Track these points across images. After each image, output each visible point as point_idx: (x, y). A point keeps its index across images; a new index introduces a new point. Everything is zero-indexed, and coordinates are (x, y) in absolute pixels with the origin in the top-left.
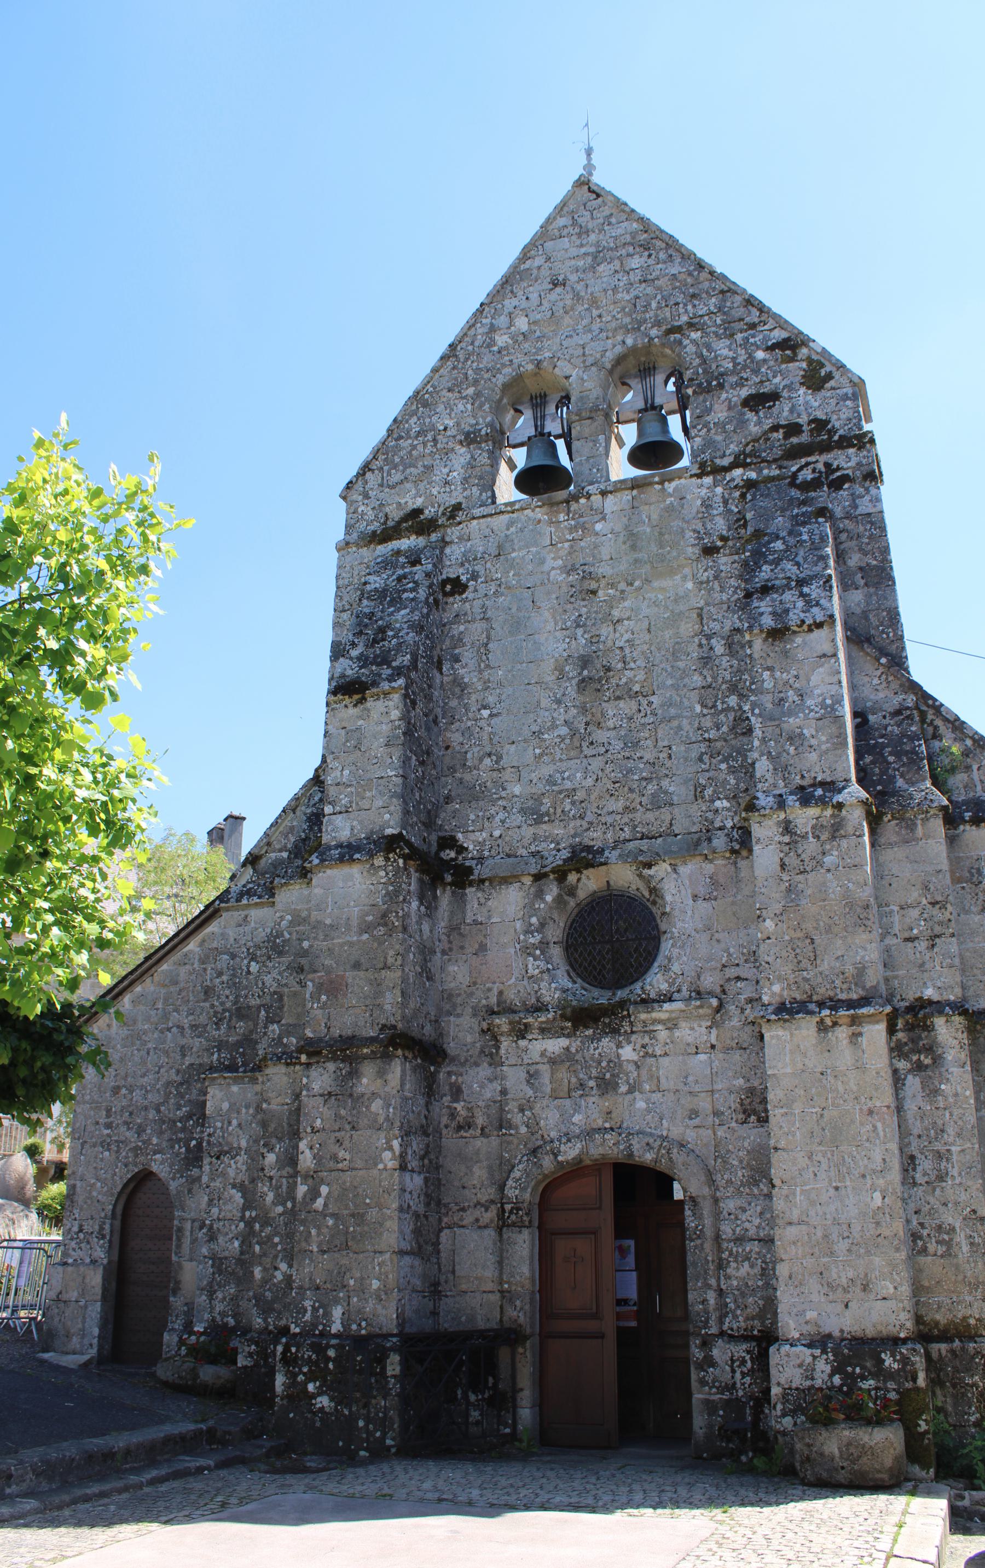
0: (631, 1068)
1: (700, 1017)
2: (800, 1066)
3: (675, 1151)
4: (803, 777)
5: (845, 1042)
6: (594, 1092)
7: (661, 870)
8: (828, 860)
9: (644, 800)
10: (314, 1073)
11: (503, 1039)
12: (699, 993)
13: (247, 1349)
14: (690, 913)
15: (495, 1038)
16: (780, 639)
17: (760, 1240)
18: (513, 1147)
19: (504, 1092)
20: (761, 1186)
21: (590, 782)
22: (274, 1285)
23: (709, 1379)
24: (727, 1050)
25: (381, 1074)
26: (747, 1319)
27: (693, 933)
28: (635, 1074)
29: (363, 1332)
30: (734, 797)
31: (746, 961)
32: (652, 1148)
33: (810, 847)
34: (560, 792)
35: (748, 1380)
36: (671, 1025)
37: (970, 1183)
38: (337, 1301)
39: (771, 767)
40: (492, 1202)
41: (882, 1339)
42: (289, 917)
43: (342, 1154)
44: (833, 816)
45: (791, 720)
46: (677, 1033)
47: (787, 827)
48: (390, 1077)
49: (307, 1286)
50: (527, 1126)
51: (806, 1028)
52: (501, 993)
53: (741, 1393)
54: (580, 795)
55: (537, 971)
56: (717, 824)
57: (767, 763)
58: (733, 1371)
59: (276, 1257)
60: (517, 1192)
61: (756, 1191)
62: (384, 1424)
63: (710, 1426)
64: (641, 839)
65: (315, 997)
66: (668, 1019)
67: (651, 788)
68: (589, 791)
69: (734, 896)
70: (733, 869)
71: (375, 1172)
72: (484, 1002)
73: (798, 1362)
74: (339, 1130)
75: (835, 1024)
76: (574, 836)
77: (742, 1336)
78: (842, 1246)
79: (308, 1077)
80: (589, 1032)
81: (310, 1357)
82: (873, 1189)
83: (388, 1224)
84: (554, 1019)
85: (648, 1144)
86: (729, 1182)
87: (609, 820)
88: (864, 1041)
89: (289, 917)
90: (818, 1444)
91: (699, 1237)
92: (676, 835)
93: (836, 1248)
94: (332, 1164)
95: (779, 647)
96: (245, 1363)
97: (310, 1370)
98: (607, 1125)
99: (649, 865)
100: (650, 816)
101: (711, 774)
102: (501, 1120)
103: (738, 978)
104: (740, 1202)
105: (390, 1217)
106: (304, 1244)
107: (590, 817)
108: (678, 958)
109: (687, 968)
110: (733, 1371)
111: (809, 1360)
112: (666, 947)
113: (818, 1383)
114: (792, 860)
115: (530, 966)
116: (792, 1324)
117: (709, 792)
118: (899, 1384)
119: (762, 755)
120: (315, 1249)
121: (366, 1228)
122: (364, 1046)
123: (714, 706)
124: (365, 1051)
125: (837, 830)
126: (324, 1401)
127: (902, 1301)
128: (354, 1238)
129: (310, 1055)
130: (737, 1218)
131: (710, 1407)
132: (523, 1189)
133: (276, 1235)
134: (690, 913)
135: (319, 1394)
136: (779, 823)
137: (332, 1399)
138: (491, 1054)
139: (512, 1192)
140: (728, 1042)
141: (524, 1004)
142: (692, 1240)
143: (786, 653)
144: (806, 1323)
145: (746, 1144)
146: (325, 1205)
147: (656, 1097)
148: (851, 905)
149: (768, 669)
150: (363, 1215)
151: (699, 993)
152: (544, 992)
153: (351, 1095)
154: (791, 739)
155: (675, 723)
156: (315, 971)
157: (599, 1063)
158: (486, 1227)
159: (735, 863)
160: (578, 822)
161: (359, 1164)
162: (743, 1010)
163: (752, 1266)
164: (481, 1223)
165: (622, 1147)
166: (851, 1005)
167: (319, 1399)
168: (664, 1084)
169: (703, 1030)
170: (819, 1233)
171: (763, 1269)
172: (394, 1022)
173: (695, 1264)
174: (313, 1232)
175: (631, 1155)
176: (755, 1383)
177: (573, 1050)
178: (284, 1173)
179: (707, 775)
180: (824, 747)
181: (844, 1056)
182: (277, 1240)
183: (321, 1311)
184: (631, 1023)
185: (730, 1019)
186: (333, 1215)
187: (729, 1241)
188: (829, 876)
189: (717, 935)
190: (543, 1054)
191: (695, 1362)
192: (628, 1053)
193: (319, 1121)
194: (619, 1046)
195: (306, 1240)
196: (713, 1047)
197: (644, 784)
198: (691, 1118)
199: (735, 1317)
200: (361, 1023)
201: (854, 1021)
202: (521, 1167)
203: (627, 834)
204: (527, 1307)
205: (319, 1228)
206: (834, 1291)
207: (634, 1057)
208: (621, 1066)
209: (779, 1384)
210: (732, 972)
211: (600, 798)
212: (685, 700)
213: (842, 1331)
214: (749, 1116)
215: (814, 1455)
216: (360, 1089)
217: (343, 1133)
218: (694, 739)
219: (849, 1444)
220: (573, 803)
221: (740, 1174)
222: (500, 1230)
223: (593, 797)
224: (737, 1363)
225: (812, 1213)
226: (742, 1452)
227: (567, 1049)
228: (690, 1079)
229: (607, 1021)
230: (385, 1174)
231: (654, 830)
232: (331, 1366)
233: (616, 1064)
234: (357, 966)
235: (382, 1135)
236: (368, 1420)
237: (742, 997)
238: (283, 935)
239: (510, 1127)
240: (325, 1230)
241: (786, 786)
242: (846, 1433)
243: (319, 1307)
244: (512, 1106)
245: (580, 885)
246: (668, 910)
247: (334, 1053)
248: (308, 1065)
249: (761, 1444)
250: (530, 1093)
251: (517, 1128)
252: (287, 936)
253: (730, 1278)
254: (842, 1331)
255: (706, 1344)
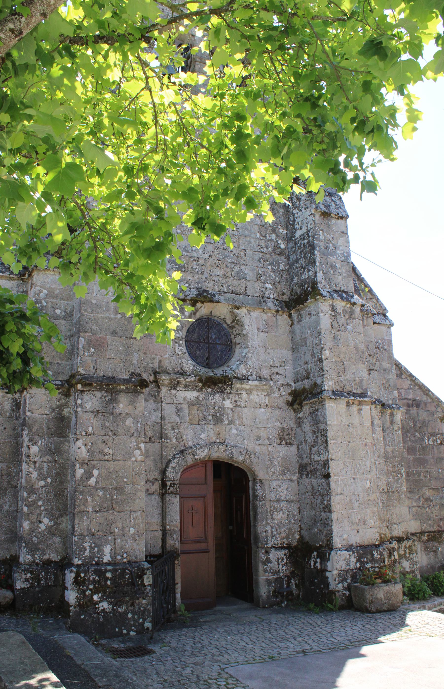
0: (229, 412)
1: (263, 390)
2: (340, 421)
3: (253, 456)
4: (336, 286)
5: (356, 412)
6: (212, 422)
7: (242, 312)
8: (349, 327)
9: (233, 273)
10: (86, 397)
11: (163, 388)
12: (260, 378)
13: (24, 576)
14: (256, 337)
15: (158, 387)
16: (327, 218)
17: (287, 501)
18: (168, 449)
19: (162, 418)
20: (287, 475)
21: (206, 256)
22: (39, 533)
23: (268, 569)
24: (273, 408)
25: (132, 402)
26: (281, 539)
27: (258, 347)
28: (231, 415)
29: (125, 560)
30: (274, 284)
31: (281, 365)
32: (242, 454)
33: (342, 319)
34: (191, 257)
35: (285, 568)
36: (249, 392)
37: (382, 477)
38: (107, 542)
39: (324, 277)
40: (156, 480)
41: (371, 545)
42: (45, 292)
43: (107, 450)
44: (350, 307)
45: (331, 258)
46: (251, 397)
47: (333, 309)
48: (138, 405)
49: (86, 533)
50: (176, 438)
51: (342, 403)
52: (160, 361)
53: (281, 574)
54: (201, 262)
55: (180, 353)
56: (267, 296)
57: (322, 275)
58: (279, 564)
59: (40, 514)
60: (174, 475)
61: (285, 478)
62: (142, 614)
63: (269, 592)
64: (232, 293)
65: (86, 348)
66: (249, 389)
67: (237, 268)
68: (206, 261)
69: (276, 333)
70: (275, 319)
71: (130, 463)
72: (151, 365)
73: (344, 558)
74: (105, 435)
75: (353, 403)
76: (198, 283)
77: (280, 547)
78: (356, 505)
79: (82, 399)
80: (210, 390)
81: (94, 579)
82: (367, 479)
83: (139, 494)
84: (194, 381)
85: (240, 452)
86: (274, 473)
87: (216, 279)
88: (362, 412)
89: (45, 292)
90: (375, 594)
91: (264, 500)
92: (249, 296)
93: (354, 505)
94: (101, 457)
95: (325, 221)
96: (23, 586)
97: (95, 587)
98: (218, 441)
99: (238, 308)
100: (236, 283)
101: (264, 269)
102: (161, 433)
103: (277, 373)
104: (279, 483)
105: (140, 490)
106: (82, 507)
107: (206, 275)
108: (251, 359)
109: (255, 364)
110: (279, 564)
111: (348, 557)
112: (238, 352)
113: (351, 567)
114: (335, 324)
115: (177, 349)
116: (338, 542)
117: (263, 278)
118: (379, 564)
119: (320, 270)
120: (91, 510)
121: (125, 497)
122: (123, 384)
123: (265, 236)
124: (122, 387)
125: (351, 315)
126: (104, 605)
127: (376, 528)
128: (117, 503)
129: (84, 385)
130: (277, 491)
131: (269, 582)
132: (177, 473)
133: (39, 500)
134: (256, 337)
135: (100, 601)
136: (330, 305)
137: (110, 603)
138: (155, 396)
139: (170, 474)
140: (273, 404)
141: (173, 370)
142: (260, 501)
143: (328, 225)
144: (344, 540)
145: (281, 455)
146: (97, 482)
147: (241, 428)
148: (357, 350)
149: (322, 230)
150: (122, 489)
151: (260, 378)
152: (184, 365)
153: (112, 414)
154: (331, 266)
155: (248, 239)
156: (86, 332)
157: (214, 408)
158: (153, 494)
159: (276, 317)
160: (200, 276)
161: (119, 457)
162: (279, 389)
163: (283, 514)
164: (150, 492)
165: (228, 453)
166: (355, 395)
167: (101, 604)
168: (245, 422)
169: (263, 396)
170: (348, 499)
171: (288, 515)
172: (139, 372)
173: (262, 513)
174: (89, 499)
175: (232, 457)
176: (288, 569)
177: (201, 399)
178: (45, 459)
179: (262, 269)
180: (344, 275)
181: (356, 420)
182: (40, 503)
183: (96, 549)
184: (231, 388)
185: (274, 393)
186: (102, 489)
187: (274, 501)
188: (349, 335)
189: (268, 350)
190: (185, 399)
191: (262, 561)
192: (228, 404)
193: (90, 429)
194: (224, 399)
195: (84, 504)
196: (267, 405)
197: (233, 265)
198: (257, 440)
199: (276, 538)
200: (118, 370)
201: (360, 403)
202: (175, 461)
203: (224, 289)
204: (179, 538)
205: (92, 496)
206: (353, 525)
207: (230, 406)
208: (224, 410)
209: (337, 569)
210: (275, 370)
211: (212, 266)
212: (252, 229)
213: (356, 543)
214: (282, 441)
215: (374, 600)
216: (118, 411)
217: (107, 437)
218: (256, 250)
219: (387, 593)
220: (198, 265)
221: (278, 469)
222: (162, 496)
223: (208, 265)
224: (280, 560)
225: (345, 490)
226: (282, 602)
227: (197, 398)
228: (257, 420)
229: (220, 385)
230: (136, 464)
231: (238, 290)
232: (109, 583)
233: (222, 408)
234: (114, 333)
235: (134, 440)
236: (134, 613)
237: (279, 383)
238: (41, 303)
239: (167, 438)
240: (97, 498)
241: (330, 288)
242: (385, 588)
243: (95, 547)
244: (167, 427)
245: (200, 310)
246: (244, 332)
247: (101, 385)
248: (82, 391)
249: (290, 597)
250: (178, 420)
251: (170, 439)
252: (45, 304)
253: (274, 519)
254: (356, 543)
255: (267, 552)
